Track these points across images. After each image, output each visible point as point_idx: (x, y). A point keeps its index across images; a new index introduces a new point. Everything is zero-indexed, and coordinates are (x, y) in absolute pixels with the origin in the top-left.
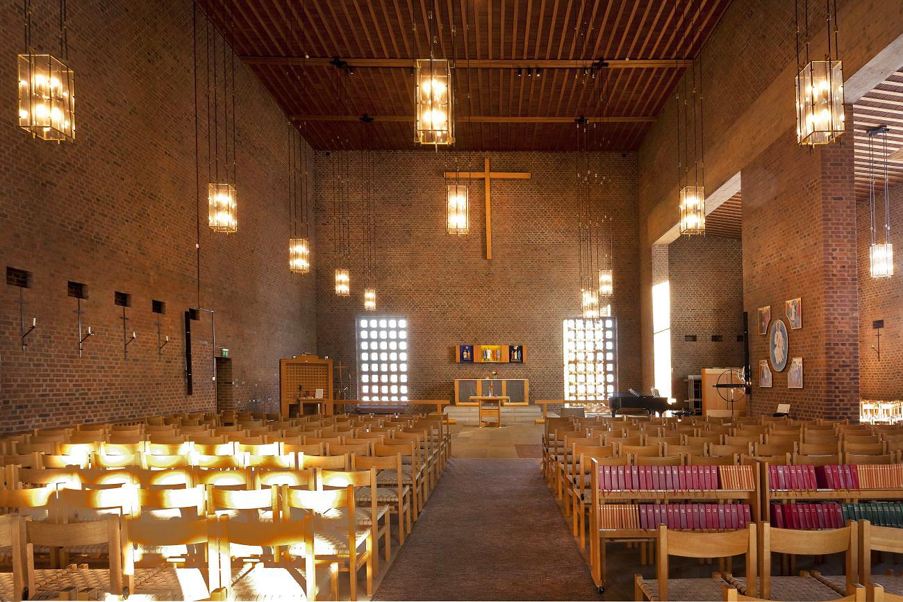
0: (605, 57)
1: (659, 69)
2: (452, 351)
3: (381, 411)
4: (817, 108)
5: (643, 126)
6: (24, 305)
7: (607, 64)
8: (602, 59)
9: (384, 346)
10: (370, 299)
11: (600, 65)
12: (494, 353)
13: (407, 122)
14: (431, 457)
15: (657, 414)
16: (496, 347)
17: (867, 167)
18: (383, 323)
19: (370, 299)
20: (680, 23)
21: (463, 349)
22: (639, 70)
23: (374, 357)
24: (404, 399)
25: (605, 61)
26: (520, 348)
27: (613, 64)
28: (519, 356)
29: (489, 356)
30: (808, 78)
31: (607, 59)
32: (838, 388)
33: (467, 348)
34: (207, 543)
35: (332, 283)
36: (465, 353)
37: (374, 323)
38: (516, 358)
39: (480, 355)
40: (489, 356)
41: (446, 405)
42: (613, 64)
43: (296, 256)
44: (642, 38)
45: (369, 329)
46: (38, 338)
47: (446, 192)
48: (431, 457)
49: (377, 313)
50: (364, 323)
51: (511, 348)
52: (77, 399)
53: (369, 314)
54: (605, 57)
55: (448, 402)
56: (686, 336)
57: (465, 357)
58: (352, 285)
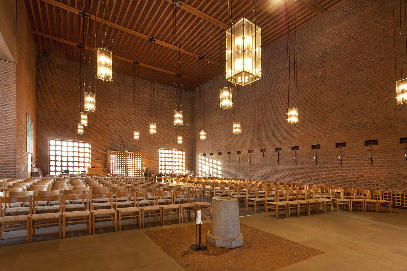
0: (154, 37)
1: (191, 56)
3: (34, 231)
4: (237, 32)
6: (317, 154)
7: (155, 41)
8: (153, 38)
13: (50, 39)
17: (267, 23)
20: (271, 28)
22: (167, 48)
25: (154, 39)
27: (158, 42)
31: (155, 38)
35: (140, 136)
42: (158, 42)
44: (153, 11)
46: (322, 161)
47: (84, 95)
52: (302, 175)
54: (154, 37)
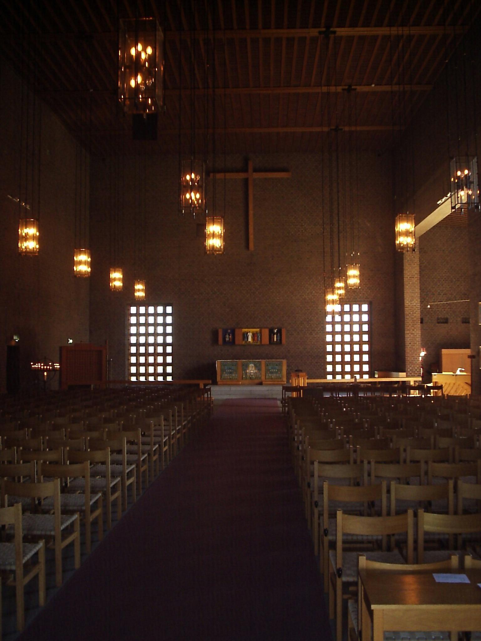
2: (215, 333)
5: (110, 482)
9: (151, 340)
10: (140, 290)
11: (349, 90)
12: (254, 335)
14: (186, 422)
15: (423, 396)
16: (255, 330)
18: (151, 310)
19: (140, 290)
21: (225, 332)
23: (142, 340)
24: (169, 379)
25: (353, 87)
26: (280, 331)
28: (278, 338)
29: (250, 339)
30: (399, 223)
32: (410, 374)
33: (229, 331)
34: (210, 388)
36: (227, 336)
37: (142, 310)
38: (275, 340)
39: (241, 337)
40: (250, 339)
41: (208, 385)
42: (359, 89)
43: (80, 263)
45: (138, 315)
48: (186, 422)
49: (145, 303)
50: (133, 310)
51: (271, 332)
53: (138, 303)
55: (211, 382)
56: (438, 319)
57: (227, 339)
58: (124, 280)
